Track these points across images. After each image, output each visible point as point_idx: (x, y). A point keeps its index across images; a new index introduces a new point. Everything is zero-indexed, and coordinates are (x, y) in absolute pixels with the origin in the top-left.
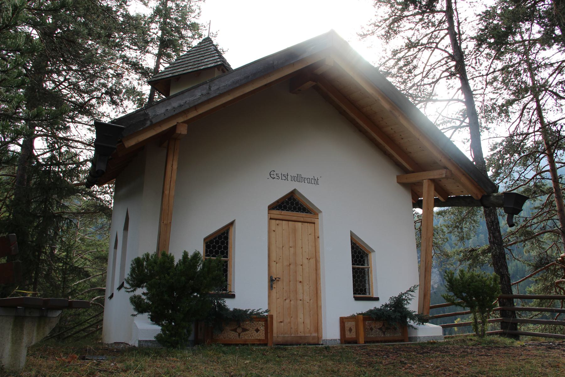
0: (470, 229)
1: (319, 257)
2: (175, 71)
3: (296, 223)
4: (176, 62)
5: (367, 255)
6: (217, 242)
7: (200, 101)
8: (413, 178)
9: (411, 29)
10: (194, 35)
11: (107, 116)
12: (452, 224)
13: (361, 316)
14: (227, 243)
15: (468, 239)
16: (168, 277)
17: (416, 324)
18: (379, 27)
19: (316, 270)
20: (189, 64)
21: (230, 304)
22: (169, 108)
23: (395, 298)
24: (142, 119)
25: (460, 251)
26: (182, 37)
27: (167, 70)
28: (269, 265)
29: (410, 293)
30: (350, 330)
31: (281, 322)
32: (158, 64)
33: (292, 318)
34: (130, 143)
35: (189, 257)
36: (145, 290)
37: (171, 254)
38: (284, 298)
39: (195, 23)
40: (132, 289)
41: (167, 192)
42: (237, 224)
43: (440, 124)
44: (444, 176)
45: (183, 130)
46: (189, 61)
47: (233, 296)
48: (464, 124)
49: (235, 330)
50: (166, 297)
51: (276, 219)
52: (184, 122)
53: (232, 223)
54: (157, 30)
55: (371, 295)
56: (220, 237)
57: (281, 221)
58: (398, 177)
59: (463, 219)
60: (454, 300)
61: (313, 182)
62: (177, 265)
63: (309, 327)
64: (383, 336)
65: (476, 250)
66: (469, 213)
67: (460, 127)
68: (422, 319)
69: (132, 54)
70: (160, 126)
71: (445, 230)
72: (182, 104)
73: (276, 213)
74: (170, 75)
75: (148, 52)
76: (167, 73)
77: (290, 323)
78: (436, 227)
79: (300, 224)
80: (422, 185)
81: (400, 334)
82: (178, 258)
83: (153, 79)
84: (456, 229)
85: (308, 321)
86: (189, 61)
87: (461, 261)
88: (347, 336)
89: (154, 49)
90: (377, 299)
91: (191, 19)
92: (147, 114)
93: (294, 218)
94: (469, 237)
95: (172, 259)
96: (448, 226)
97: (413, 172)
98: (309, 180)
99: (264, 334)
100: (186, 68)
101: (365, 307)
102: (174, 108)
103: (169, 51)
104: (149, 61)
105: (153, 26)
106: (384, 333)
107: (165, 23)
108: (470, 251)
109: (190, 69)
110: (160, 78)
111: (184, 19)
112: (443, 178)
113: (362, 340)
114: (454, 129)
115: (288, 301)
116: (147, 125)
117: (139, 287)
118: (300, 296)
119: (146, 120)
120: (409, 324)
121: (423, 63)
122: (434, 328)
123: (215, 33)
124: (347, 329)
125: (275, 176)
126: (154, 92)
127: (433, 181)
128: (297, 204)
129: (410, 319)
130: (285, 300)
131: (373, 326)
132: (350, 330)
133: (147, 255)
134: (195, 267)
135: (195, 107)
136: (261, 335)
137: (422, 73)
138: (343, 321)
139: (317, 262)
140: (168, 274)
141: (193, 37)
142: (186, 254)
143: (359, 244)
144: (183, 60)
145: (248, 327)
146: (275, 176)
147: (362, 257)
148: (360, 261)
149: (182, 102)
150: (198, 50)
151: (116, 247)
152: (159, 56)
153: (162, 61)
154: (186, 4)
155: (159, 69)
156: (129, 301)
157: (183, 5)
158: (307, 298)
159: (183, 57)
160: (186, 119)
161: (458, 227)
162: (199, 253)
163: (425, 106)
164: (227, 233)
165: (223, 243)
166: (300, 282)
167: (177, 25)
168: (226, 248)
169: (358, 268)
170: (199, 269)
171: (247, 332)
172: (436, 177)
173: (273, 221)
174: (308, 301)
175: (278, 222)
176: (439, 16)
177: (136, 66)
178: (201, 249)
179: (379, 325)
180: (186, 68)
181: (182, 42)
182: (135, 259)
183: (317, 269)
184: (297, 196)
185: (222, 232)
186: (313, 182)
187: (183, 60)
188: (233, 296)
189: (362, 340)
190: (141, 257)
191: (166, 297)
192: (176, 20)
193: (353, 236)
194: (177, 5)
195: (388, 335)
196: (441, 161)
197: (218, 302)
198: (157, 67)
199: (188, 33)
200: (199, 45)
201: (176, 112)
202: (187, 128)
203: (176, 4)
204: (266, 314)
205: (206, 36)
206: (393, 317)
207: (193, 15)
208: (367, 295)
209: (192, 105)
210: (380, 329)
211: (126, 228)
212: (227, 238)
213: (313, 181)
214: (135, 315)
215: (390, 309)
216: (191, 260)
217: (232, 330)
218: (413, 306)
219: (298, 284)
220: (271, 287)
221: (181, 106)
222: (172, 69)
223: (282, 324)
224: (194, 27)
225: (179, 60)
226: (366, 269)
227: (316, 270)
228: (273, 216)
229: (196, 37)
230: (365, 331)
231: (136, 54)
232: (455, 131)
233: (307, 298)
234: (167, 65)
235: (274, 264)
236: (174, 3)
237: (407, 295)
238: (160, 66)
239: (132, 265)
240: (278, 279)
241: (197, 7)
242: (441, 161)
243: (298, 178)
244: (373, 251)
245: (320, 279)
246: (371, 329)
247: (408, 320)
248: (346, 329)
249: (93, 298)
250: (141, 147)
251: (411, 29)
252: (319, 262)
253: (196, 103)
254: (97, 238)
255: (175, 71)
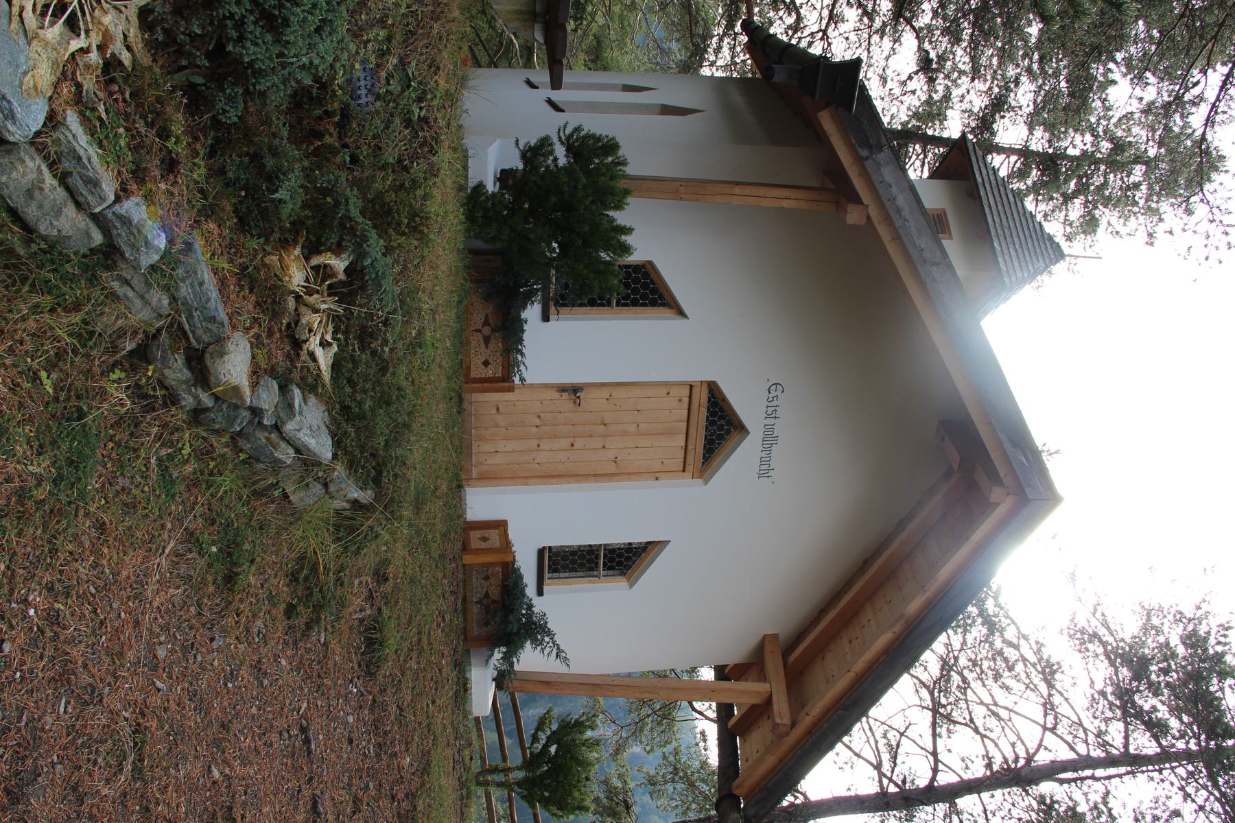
0: (672, 799)
1: (619, 481)
2: (988, 188)
3: (684, 436)
4: (1008, 191)
5: (623, 574)
6: (645, 286)
7: (909, 246)
8: (774, 665)
9: (1092, 682)
10: (1070, 225)
11: (893, 49)
12: (682, 761)
13: (510, 559)
14: (644, 305)
15: (651, 794)
16: (587, 202)
17: (496, 663)
18: (1094, 614)
19: (595, 475)
20: (1003, 217)
21: (532, 313)
22: (894, 189)
23: (546, 623)
24: (871, 141)
25: (625, 781)
26: (1067, 198)
27: (991, 172)
28: (603, 385)
29: (555, 652)
30: (485, 539)
31: (498, 409)
32: (1008, 151)
33: (504, 430)
34: (826, 121)
35: (623, 238)
36: (562, 161)
37: (627, 204)
38: (542, 415)
39: (1097, 226)
40: (563, 138)
41: (737, 190)
42: (681, 322)
43: (889, 740)
44: (778, 721)
45: (853, 216)
46: (1010, 217)
47: (546, 318)
48: (885, 781)
49: (486, 323)
50: (553, 200)
51: (690, 397)
52: (869, 218)
53: (681, 313)
54: (1081, 146)
55: (547, 581)
56: (655, 291)
57: (687, 407)
58: (775, 636)
59: (692, 784)
60: (543, 731)
61: (762, 467)
62: (608, 216)
63: (488, 462)
64: (475, 600)
65: (628, 813)
66: (706, 798)
67: (881, 775)
68: (501, 681)
69: (1025, 95)
70: (860, 174)
71: (669, 748)
72: (903, 214)
73: (702, 397)
74: (979, 180)
75: (1031, 130)
76: (984, 172)
77: (497, 426)
78: (675, 729)
79: (683, 443)
80: (759, 681)
81: (476, 633)
82: (620, 217)
83: (969, 144)
84: (670, 769)
85: (499, 459)
86: (1010, 217)
87: (606, 782)
88: (472, 533)
89: (1039, 141)
90: (540, 592)
91: (1106, 216)
92: (881, 150)
93: (692, 431)
94: (655, 795)
95: (619, 207)
96: (677, 753)
97: (785, 665)
98: (765, 460)
99: (479, 376)
100: (995, 212)
101: (527, 566)
102: (895, 199)
103: (1035, 173)
104: (1010, 132)
105: (1088, 138)
106: (479, 602)
107: (1097, 162)
108: (625, 801)
109: (994, 221)
110: (973, 159)
111: (1107, 201)
112: (773, 720)
113: (468, 559)
114: (875, 763)
115: (537, 421)
116: (860, 150)
117: (566, 150)
118: (546, 445)
119: (870, 148)
120: (496, 650)
121: (1016, 703)
122: (487, 701)
123: (1076, 269)
124: (486, 533)
125: (773, 394)
126: (947, 146)
127: (769, 702)
128: (721, 437)
129: (504, 653)
130: (539, 417)
131: (493, 581)
132: (485, 539)
133: (624, 163)
134: (606, 249)
135: (897, 238)
136: (478, 371)
137: (995, 704)
138: (501, 525)
139: (610, 476)
140: (593, 202)
141: (1067, 222)
142: (627, 231)
143: (645, 558)
144: (1013, 205)
145: (492, 346)
146: (773, 394)
147: (620, 563)
148: (612, 560)
149: (906, 213)
150: (1036, 233)
151: (628, 88)
152: (1025, 153)
153: (1013, 158)
154: (1141, 205)
155: (994, 155)
156: (543, 135)
157: (1136, 198)
158: (542, 457)
159: (1019, 204)
160: (875, 220)
161: (676, 774)
162: (630, 254)
163: (923, 708)
164: (663, 305)
165: (644, 297)
166: (572, 445)
167: (1092, 188)
168: (635, 303)
169: (597, 557)
170: (602, 255)
171: (483, 344)
172: (775, 706)
173: (687, 392)
174: (537, 461)
175: (686, 400)
176: (1115, 733)
177: (998, 105)
178: (636, 257)
179: (495, 592)
180: (995, 212)
181: (1057, 199)
182: (617, 143)
183: (597, 476)
184: (735, 437)
185: (666, 295)
186: (762, 467)
187: (1013, 205)
188: (546, 318)
189: (468, 559)
190: (620, 153)
191: (553, 200)
192: (1105, 185)
193: (661, 544)
194: (1136, 186)
195: (475, 609)
196: (807, 714)
197: (537, 290)
198: (1000, 150)
199: (1076, 210)
200: (1046, 237)
201: (887, 204)
202: (858, 223)
203: (1140, 184)
204: (517, 380)
205: (1066, 251)
206: (511, 618)
207: (1114, 220)
208: (547, 575)
209: (901, 231)
210: (487, 595)
211: (667, 110)
212: (653, 303)
213: (765, 467)
214: (517, 144)
215: (523, 615)
216: (619, 241)
217: (486, 317)
218: (530, 659)
219: (569, 441)
220: (562, 389)
221: (899, 211)
222: (993, 182)
223: (494, 411)
224: (1090, 224)
225: (1014, 197)
226: (596, 573)
227: (595, 475)
228: (696, 391)
229: (1068, 229)
230: (483, 565)
231: (1025, 106)
232: (872, 764)
233: (542, 457)
234: (1003, 173)
235: (605, 393)
236: (1141, 179)
237: (551, 644)
238: (1003, 157)
239: (607, 136)
240: (577, 401)
241: (1134, 229)
242: (807, 714)
243: (770, 438)
244: (631, 586)
245: (579, 482)
246: (487, 578)
247: (503, 649)
248: (486, 531)
249: (514, 34)
250: (821, 138)
251: (1092, 682)
252: (610, 481)
253: (905, 239)
254: (639, 38)
255: (988, 188)
